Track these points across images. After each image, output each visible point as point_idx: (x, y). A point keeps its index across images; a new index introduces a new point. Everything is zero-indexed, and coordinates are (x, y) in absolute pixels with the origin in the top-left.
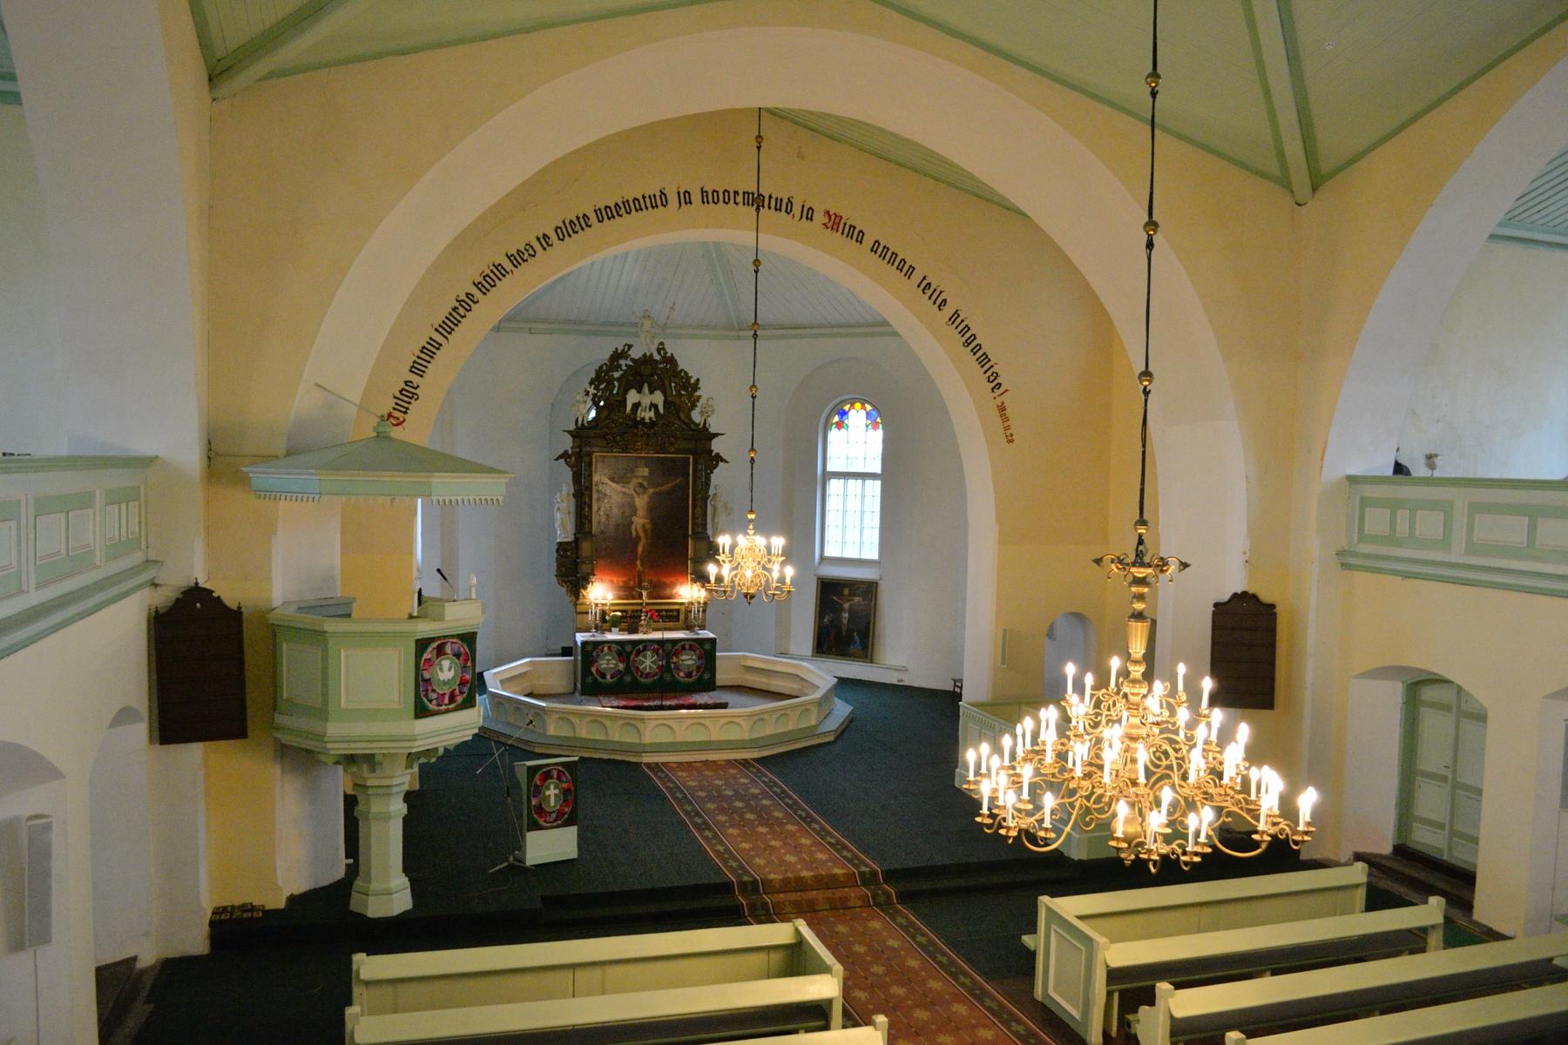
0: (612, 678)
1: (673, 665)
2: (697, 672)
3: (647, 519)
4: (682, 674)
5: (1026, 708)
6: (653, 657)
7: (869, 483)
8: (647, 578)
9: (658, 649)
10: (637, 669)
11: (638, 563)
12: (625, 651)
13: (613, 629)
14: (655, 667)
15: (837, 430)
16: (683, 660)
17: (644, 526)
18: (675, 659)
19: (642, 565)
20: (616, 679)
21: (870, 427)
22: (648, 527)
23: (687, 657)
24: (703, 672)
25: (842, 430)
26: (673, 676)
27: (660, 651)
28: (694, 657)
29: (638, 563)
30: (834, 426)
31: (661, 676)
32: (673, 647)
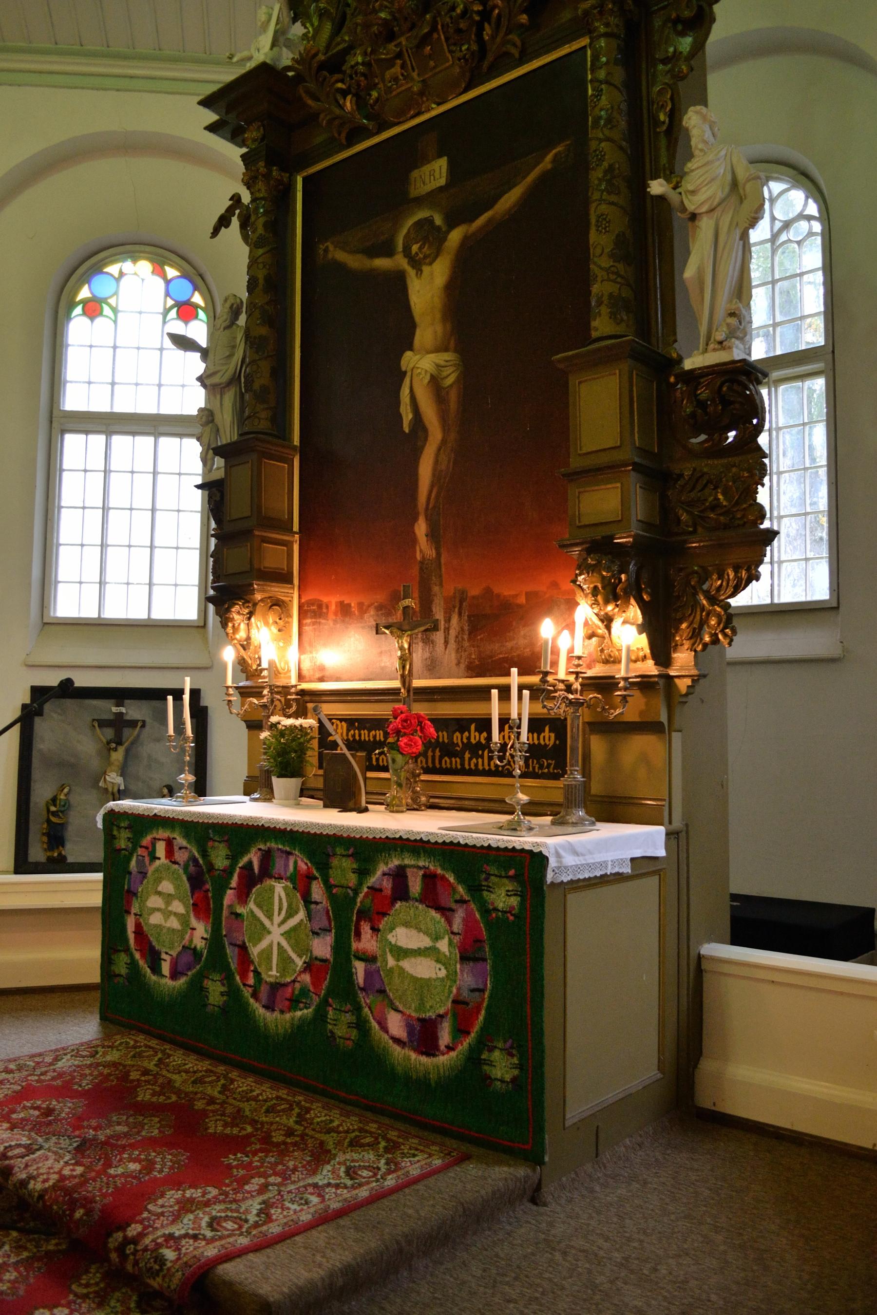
0: (174, 975)
1: (359, 968)
2: (461, 1030)
3: (442, 348)
4: (396, 1025)
5: (399, 1068)
6: (290, 914)
7: (168, 443)
8: (450, 588)
9: (310, 878)
10: (243, 949)
11: (421, 528)
12: (211, 867)
13: (279, 784)
14: (300, 962)
15: (85, 320)
16: (401, 953)
17: (435, 381)
18: (367, 942)
19: (433, 535)
20: (183, 980)
21: (173, 313)
22: (450, 378)
23: (421, 941)
24: (484, 1043)
25: (99, 320)
26: (361, 1025)
27: (317, 891)
28: (443, 945)
29: (421, 528)
30: (78, 310)
31: (320, 1016)
32: (234, 858)
